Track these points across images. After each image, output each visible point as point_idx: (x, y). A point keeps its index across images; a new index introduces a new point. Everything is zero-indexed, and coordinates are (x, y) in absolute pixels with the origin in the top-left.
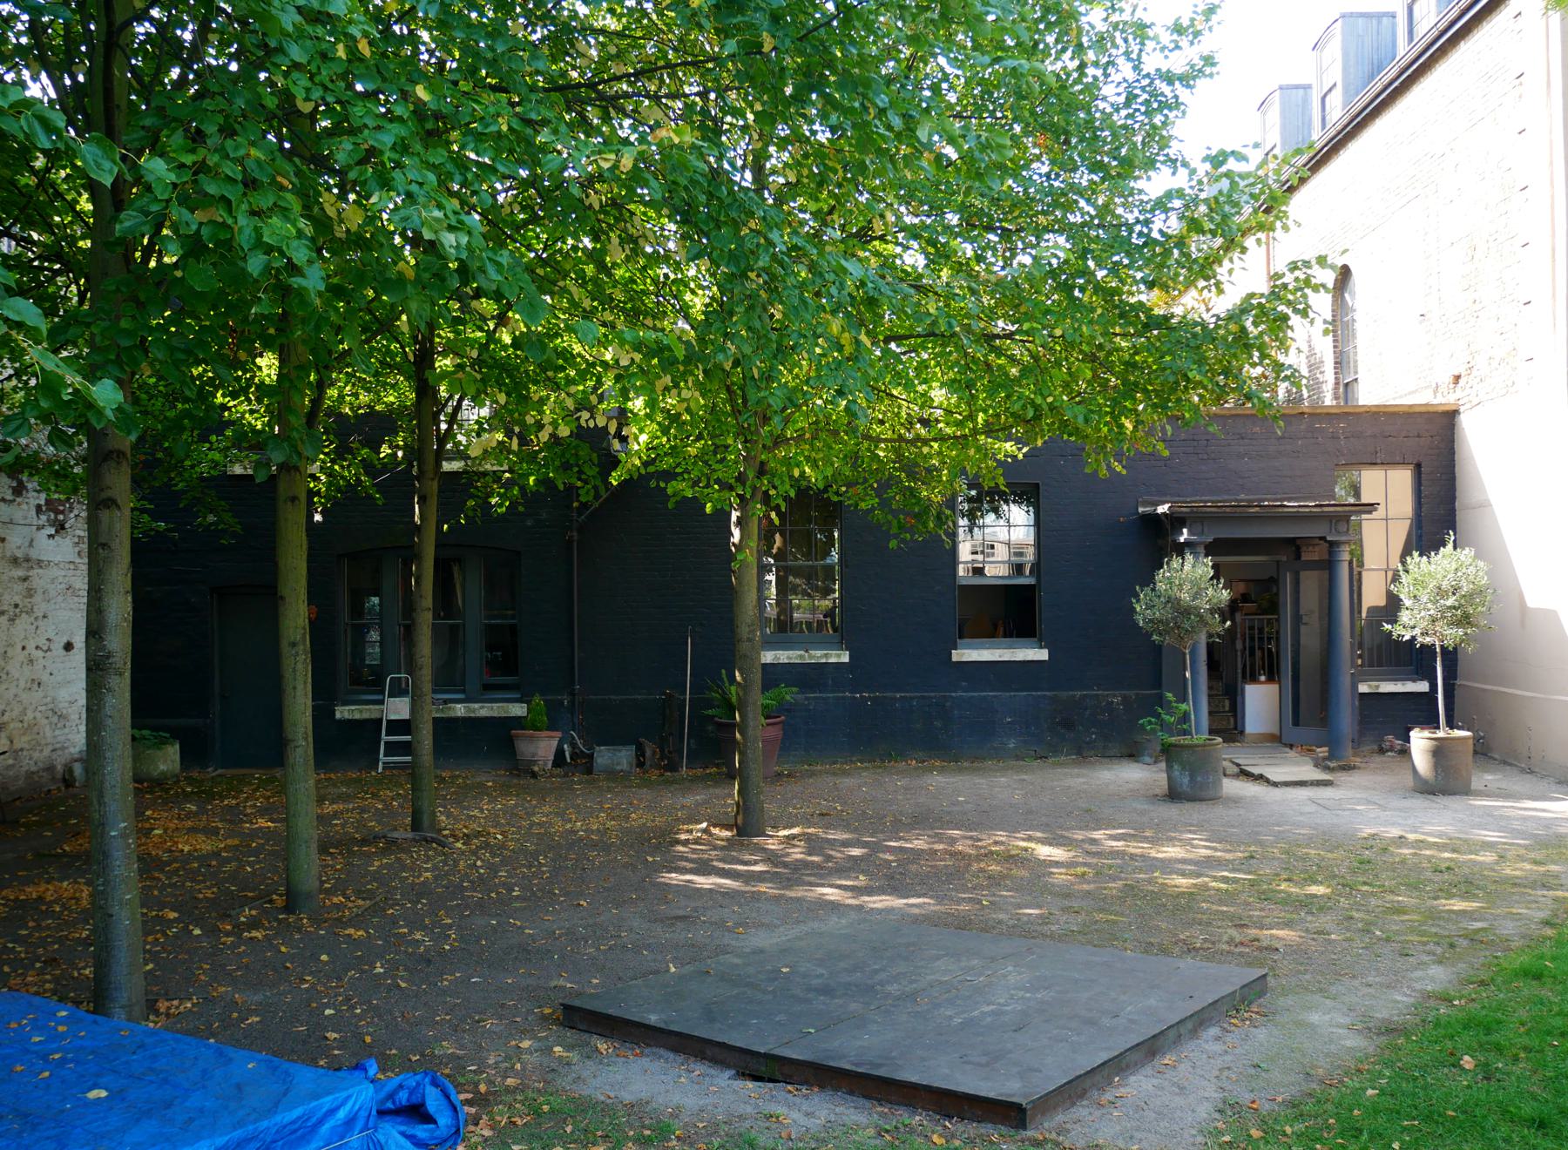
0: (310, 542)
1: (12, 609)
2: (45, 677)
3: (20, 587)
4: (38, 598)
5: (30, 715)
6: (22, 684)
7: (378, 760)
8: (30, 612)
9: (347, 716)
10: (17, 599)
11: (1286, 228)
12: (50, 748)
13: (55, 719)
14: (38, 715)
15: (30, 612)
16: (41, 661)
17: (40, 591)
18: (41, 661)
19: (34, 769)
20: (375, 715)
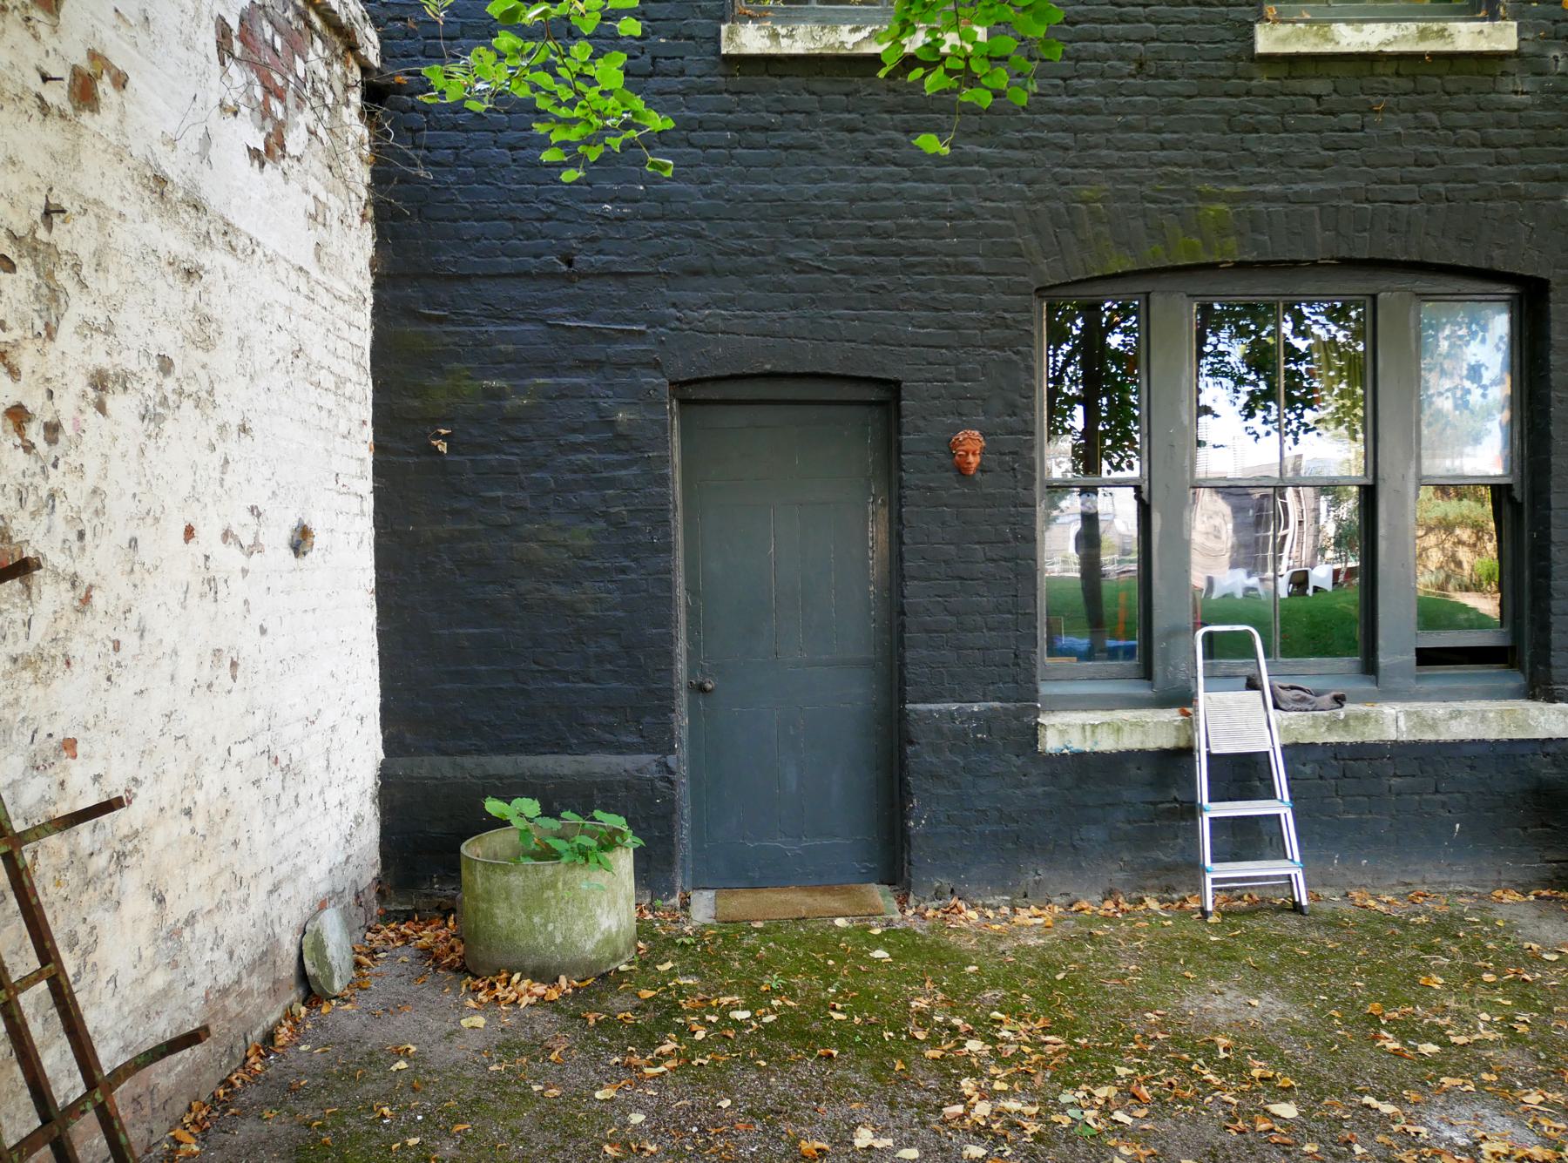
0: (376, 297)
1: (151, 374)
2: (247, 644)
3: (173, 295)
4: (224, 359)
5: (212, 780)
6: (188, 671)
7: (1192, 810)
8: (205, 401)
9: (1078, 743)
10: (167, 340)
11: (1483, 341)
12: (266, 883)
13: (273, 785)
14: (234, 776)
15: (205, 401)
16: (237, 584)
17: (231, 336)
18: (237, 584)
19: (225, 976)
20: (1167, 741)
